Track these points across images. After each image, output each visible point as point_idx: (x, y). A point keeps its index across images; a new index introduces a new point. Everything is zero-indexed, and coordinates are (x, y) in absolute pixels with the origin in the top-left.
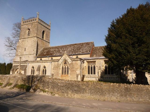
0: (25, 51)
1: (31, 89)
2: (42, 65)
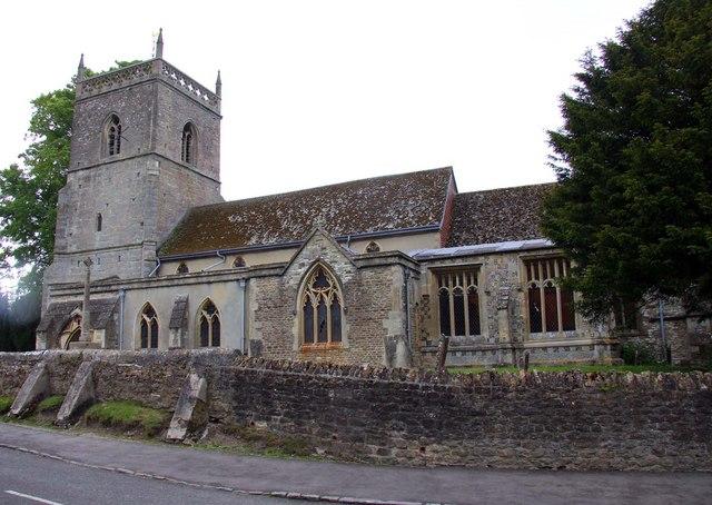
0: (99, 229)
1: (174, 424)
2: (197, 297)
